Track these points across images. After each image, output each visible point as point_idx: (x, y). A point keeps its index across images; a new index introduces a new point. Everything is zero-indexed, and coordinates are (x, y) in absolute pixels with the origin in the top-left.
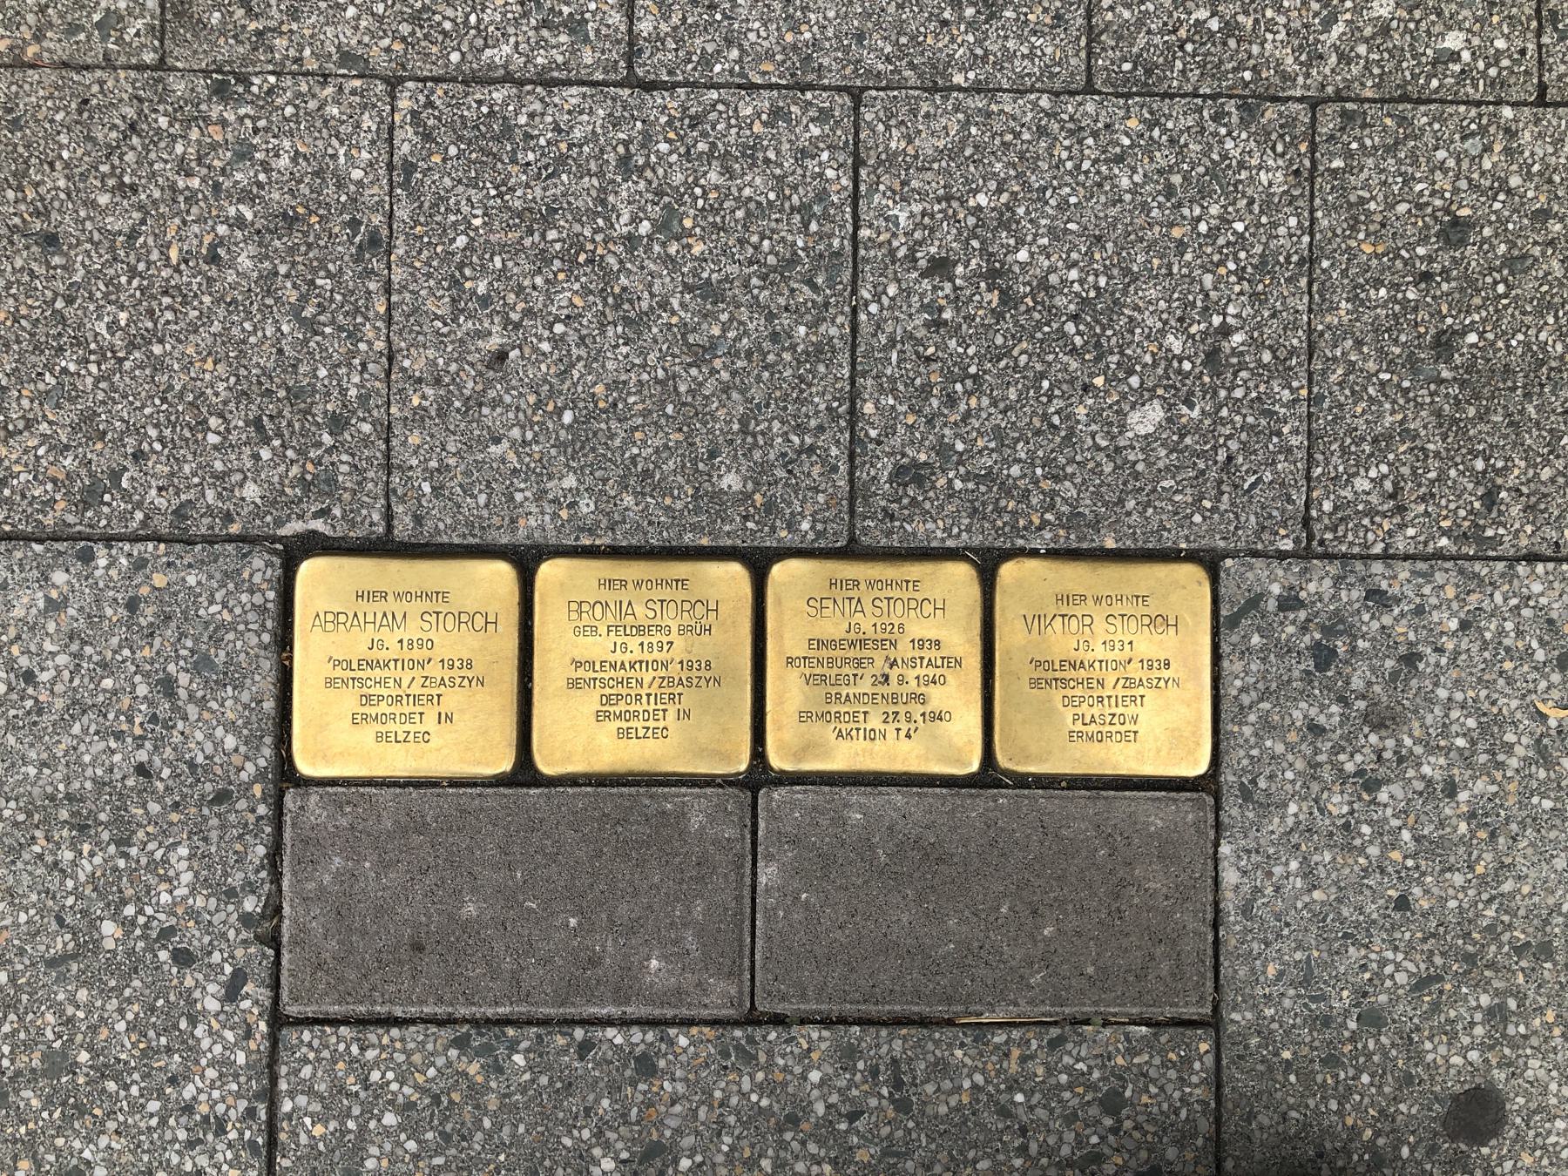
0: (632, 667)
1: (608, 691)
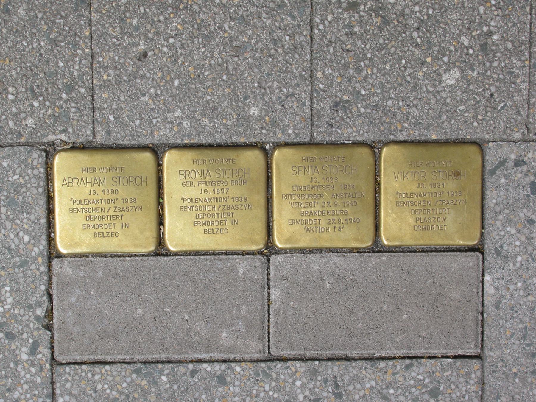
0: (210, 200)
1: (199, 212)
